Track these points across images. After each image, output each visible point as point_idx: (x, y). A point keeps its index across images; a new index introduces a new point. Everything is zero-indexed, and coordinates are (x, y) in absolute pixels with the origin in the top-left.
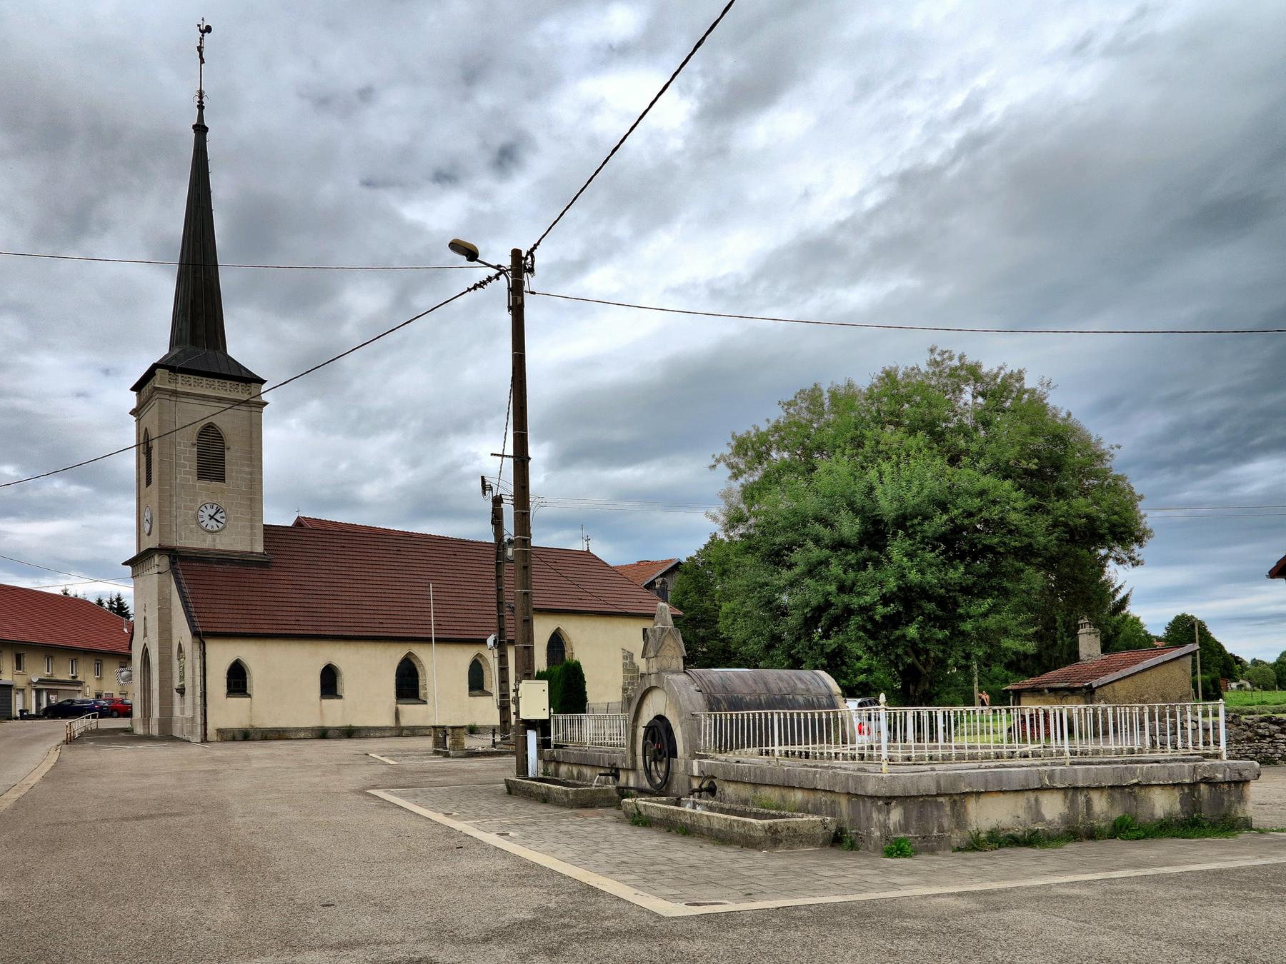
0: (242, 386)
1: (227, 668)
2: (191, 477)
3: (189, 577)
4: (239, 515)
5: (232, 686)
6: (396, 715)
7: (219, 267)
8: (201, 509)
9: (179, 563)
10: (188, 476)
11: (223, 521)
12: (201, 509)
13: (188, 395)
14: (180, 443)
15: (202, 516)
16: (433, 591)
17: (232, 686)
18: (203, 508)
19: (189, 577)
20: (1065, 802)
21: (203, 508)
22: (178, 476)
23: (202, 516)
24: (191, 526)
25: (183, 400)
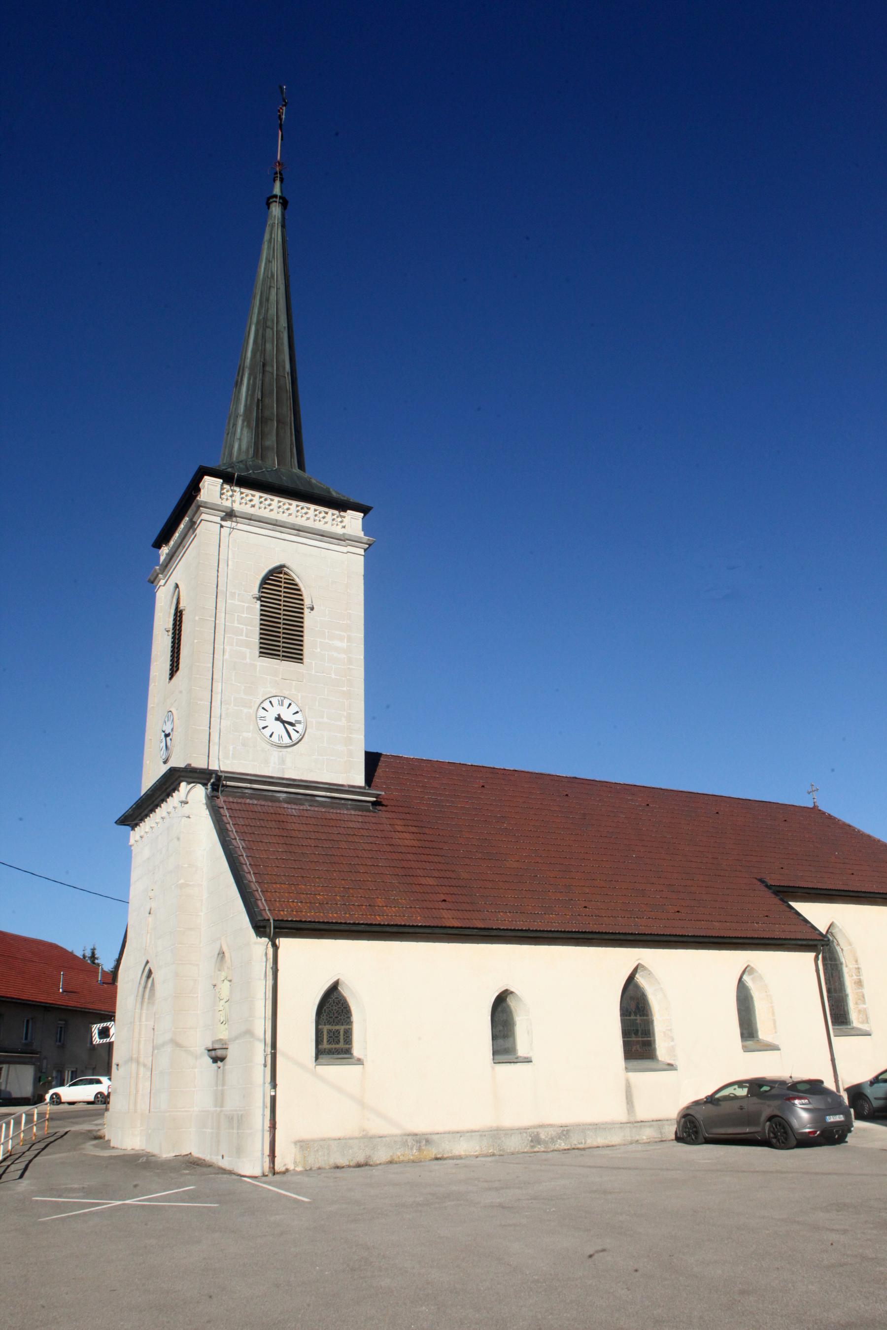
0: (333, 515)
1: (833, 1147)
2: (248, 651)
3: (241, 821)
4: (325, 720)
5: (342, 1033)
6: (627, 1098)
7: (210, 768)
8: (263, 705)
9: (222, 799)
10: (244, 649)
11: (298, 717)
12: (263, 705)
13: (250, 518)
14: (233, 595)
15: (263, 718)
16: (275, 928)
17: (342, 1033)
18: (266, 705)
19: (241, 821)
20: (740, 1084)
21: (266, 705)
22: (228, 648)
23: (263, 718)
24: (245, 735)
25: (240, 526)
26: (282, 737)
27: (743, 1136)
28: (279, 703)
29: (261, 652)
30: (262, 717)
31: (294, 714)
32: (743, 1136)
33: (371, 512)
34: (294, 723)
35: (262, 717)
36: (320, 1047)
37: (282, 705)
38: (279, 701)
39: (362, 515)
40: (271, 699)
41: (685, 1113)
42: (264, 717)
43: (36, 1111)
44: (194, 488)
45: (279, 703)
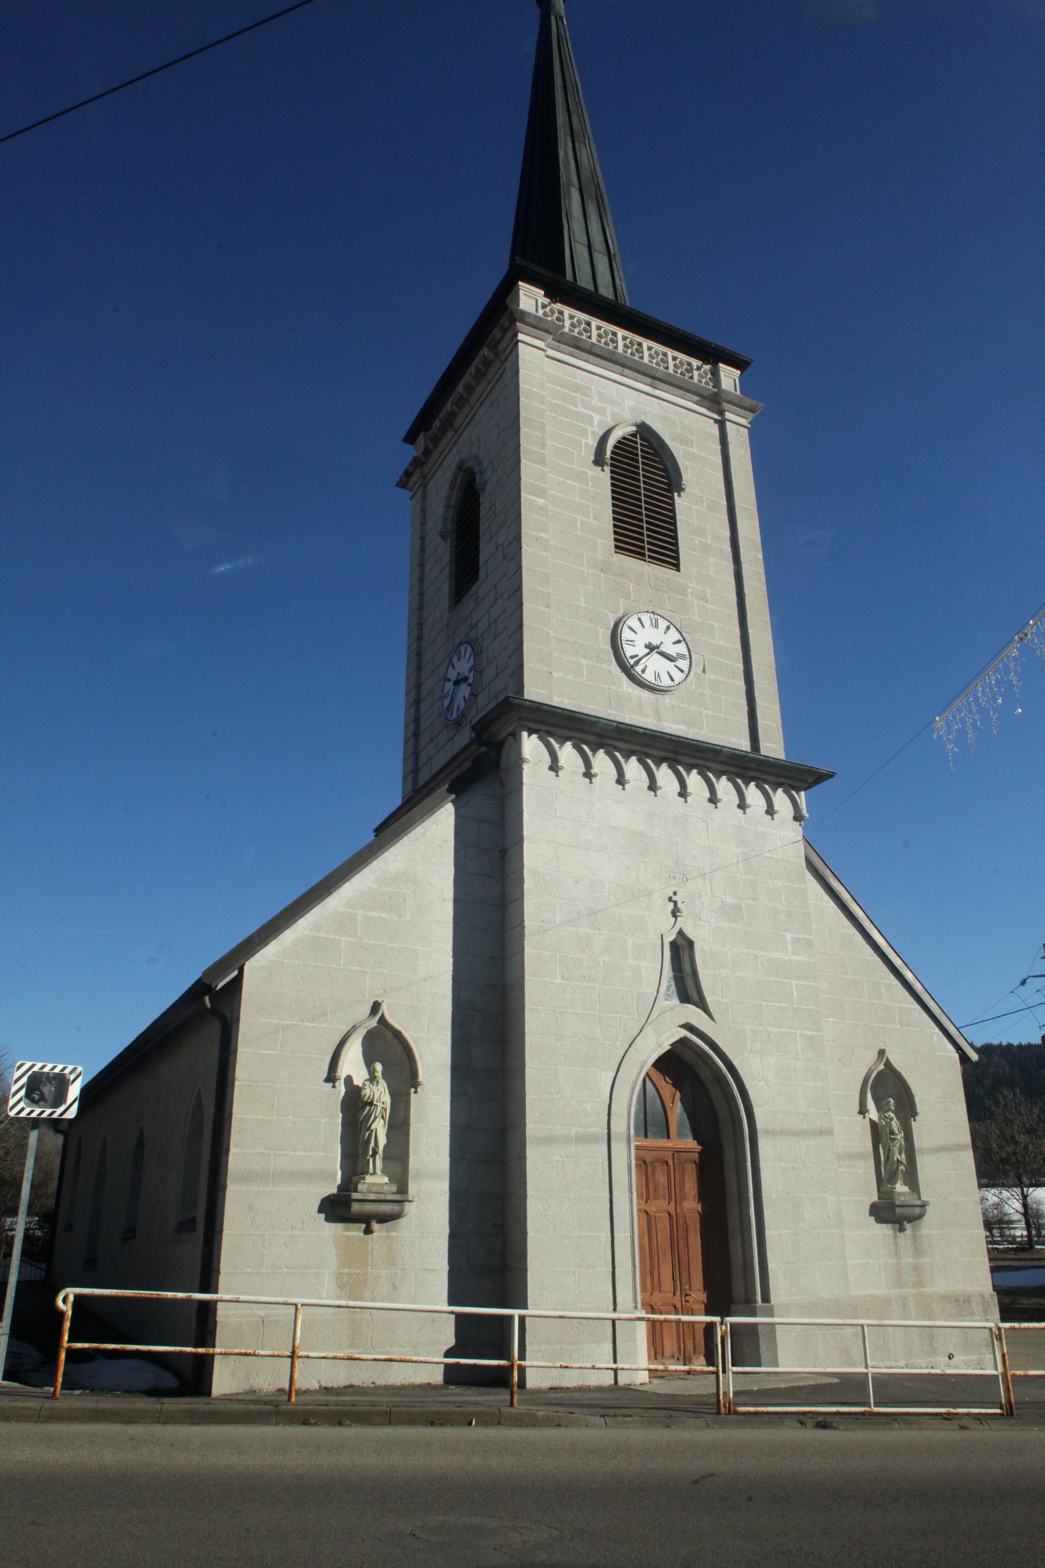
26: (659, 675)
27: (623, 1236)
28: (652, 623)
29: (616, 547)
30: (628, 641)
31: (636, 633)
32: (623, 1236)
33: (749, 369)
34: (675, 656)
35: (628, 641)
36: (883, 1189)
37: (657, 626)
38: (651, 621)
39: (739, 372)
40: (671, 626)
41: (919, 1221)
42: (631, 641)
43: (518, 1362)
44: (507, 290)
45: (652, 623)
